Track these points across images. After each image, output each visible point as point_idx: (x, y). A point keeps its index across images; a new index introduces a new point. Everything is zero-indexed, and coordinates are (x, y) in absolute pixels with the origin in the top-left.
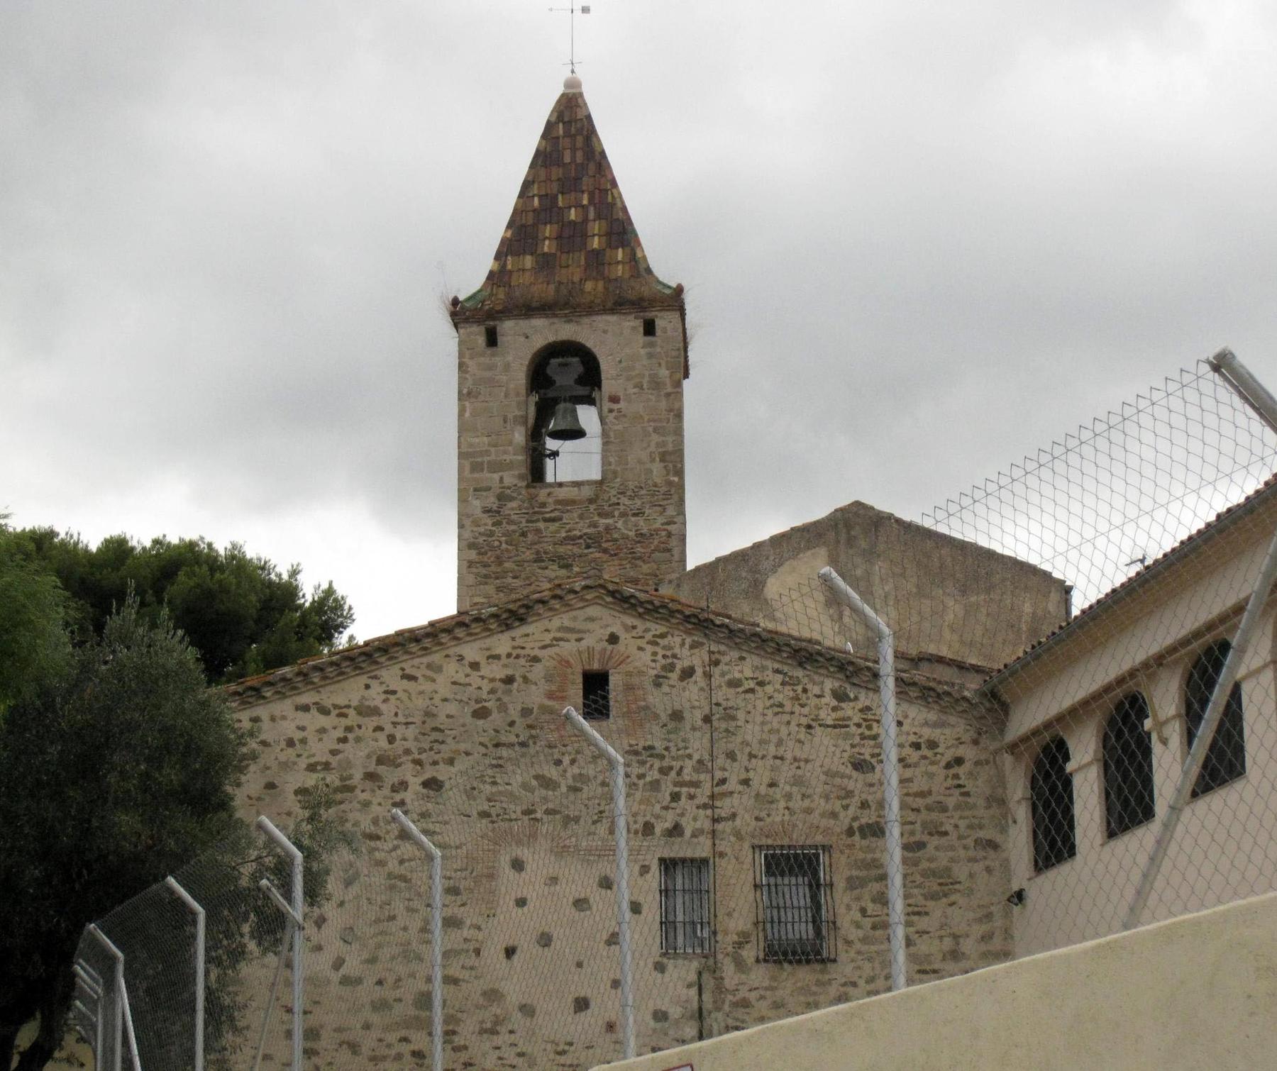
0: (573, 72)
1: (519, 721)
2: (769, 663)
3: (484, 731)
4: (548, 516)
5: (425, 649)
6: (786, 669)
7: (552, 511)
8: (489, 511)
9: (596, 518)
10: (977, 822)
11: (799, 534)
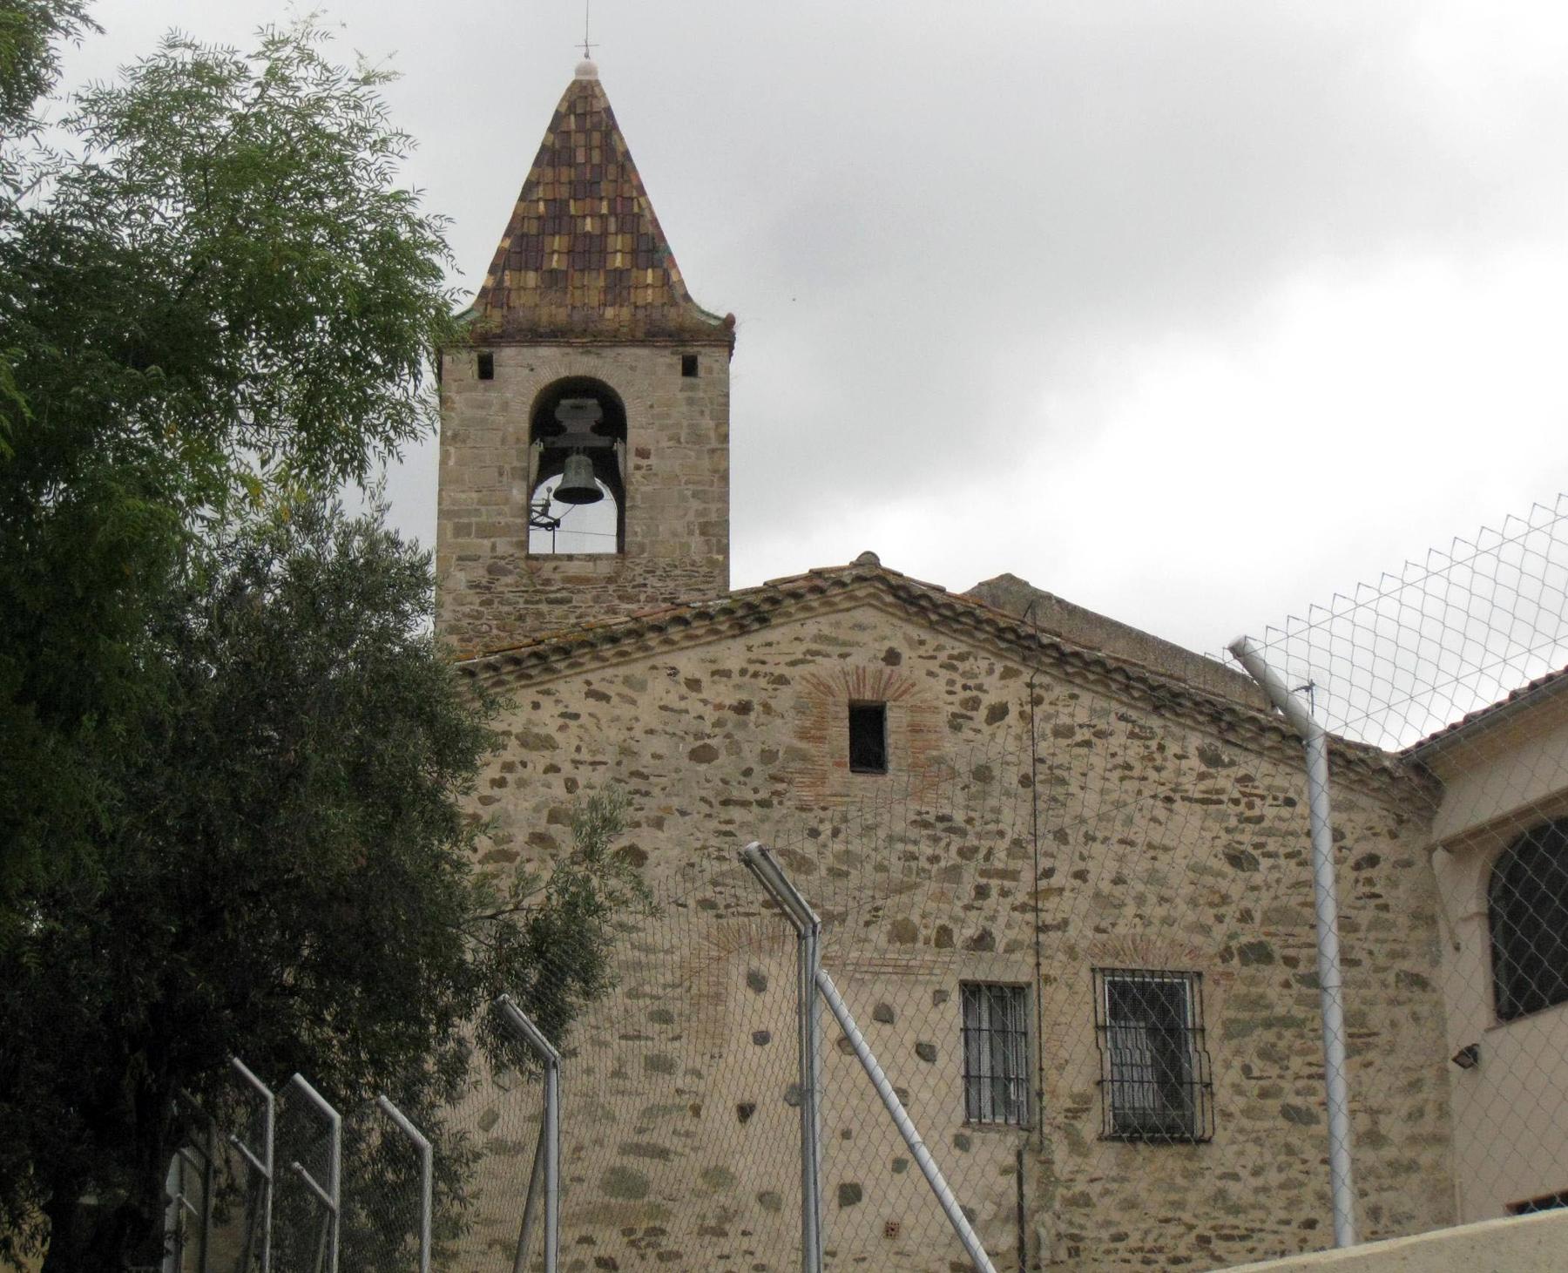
0: (587, 56)
1: (757, 768)
2: (1114, 705)
3: (708, 781)
4: (552, 596)
5: (623, 654)
6: (1133, 714)
7: (558, 590)
8: (477, 586)
9: (616, 602)
10: (1398, 947)
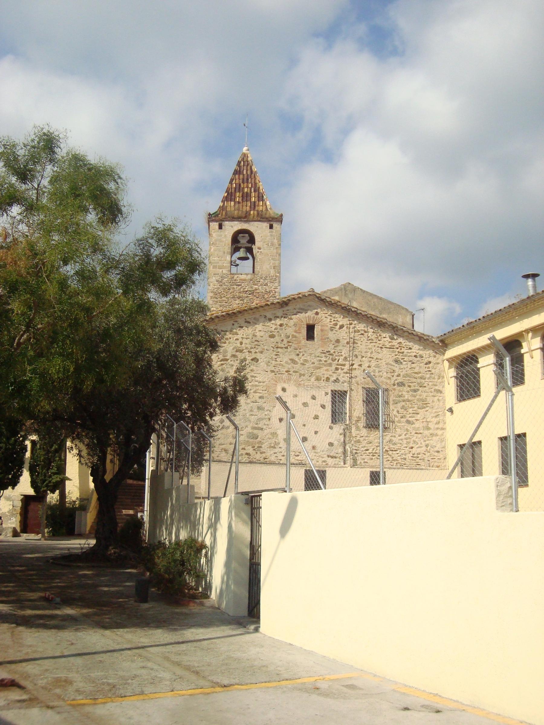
11: (330, 292)
